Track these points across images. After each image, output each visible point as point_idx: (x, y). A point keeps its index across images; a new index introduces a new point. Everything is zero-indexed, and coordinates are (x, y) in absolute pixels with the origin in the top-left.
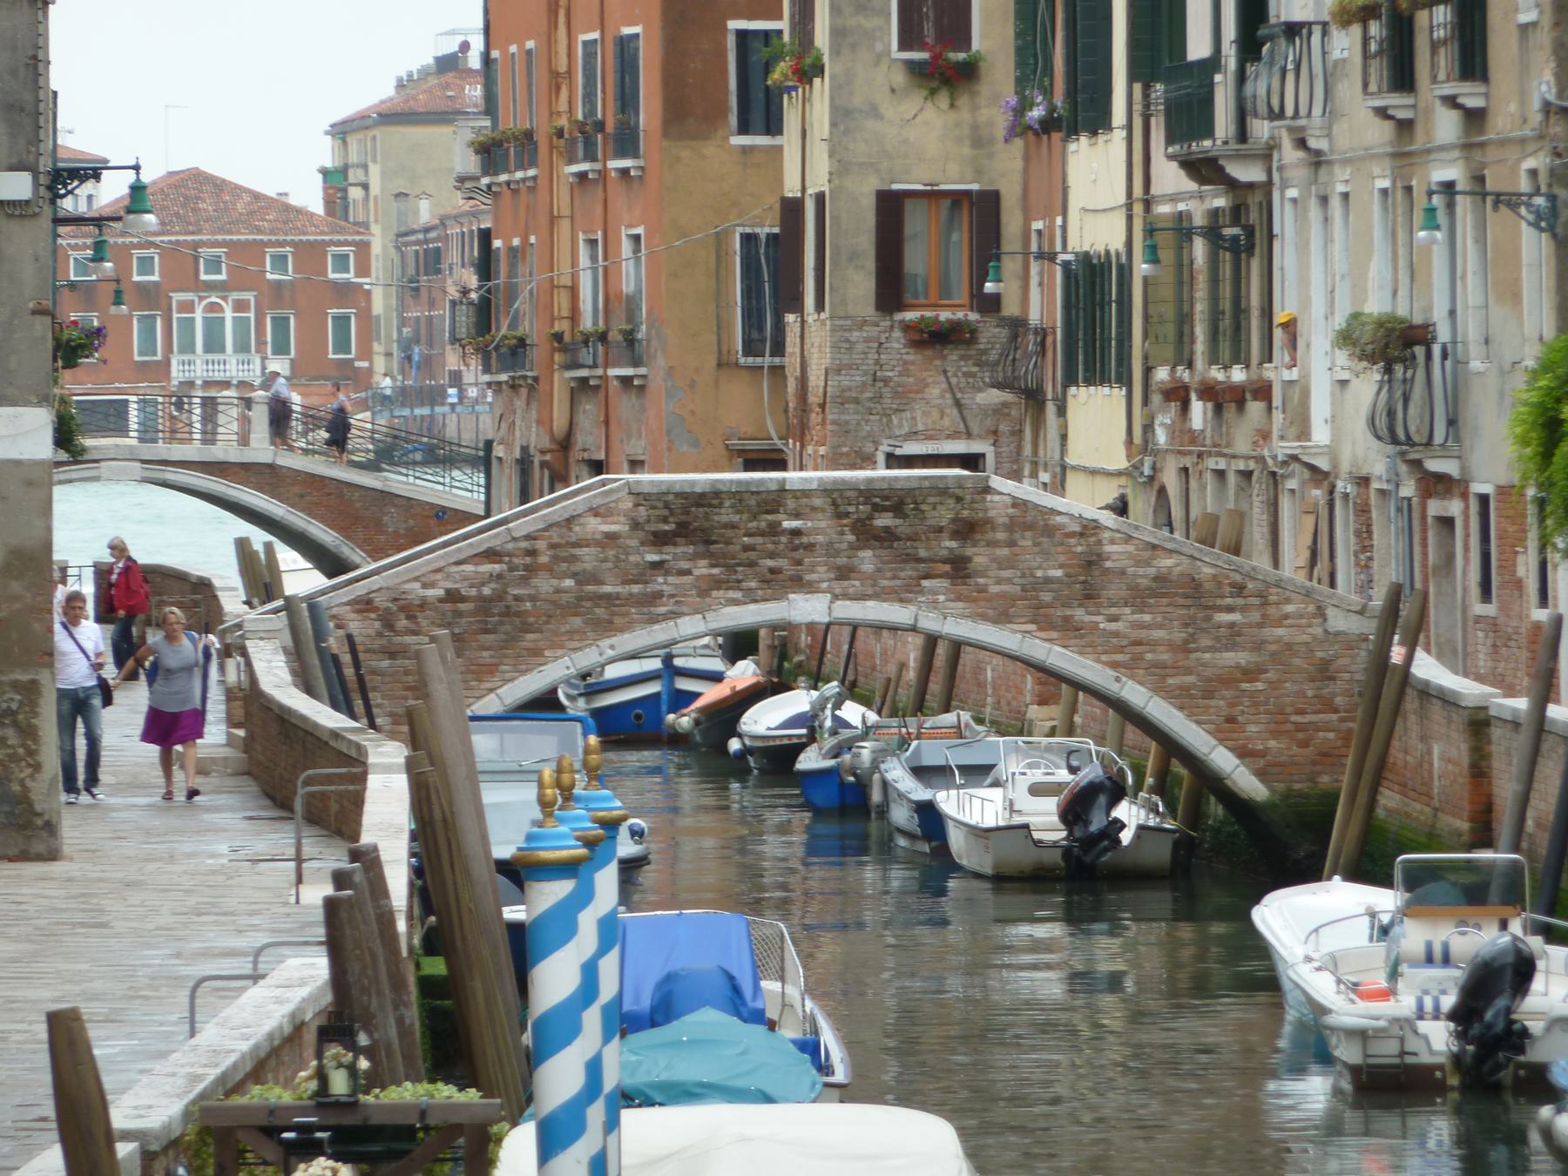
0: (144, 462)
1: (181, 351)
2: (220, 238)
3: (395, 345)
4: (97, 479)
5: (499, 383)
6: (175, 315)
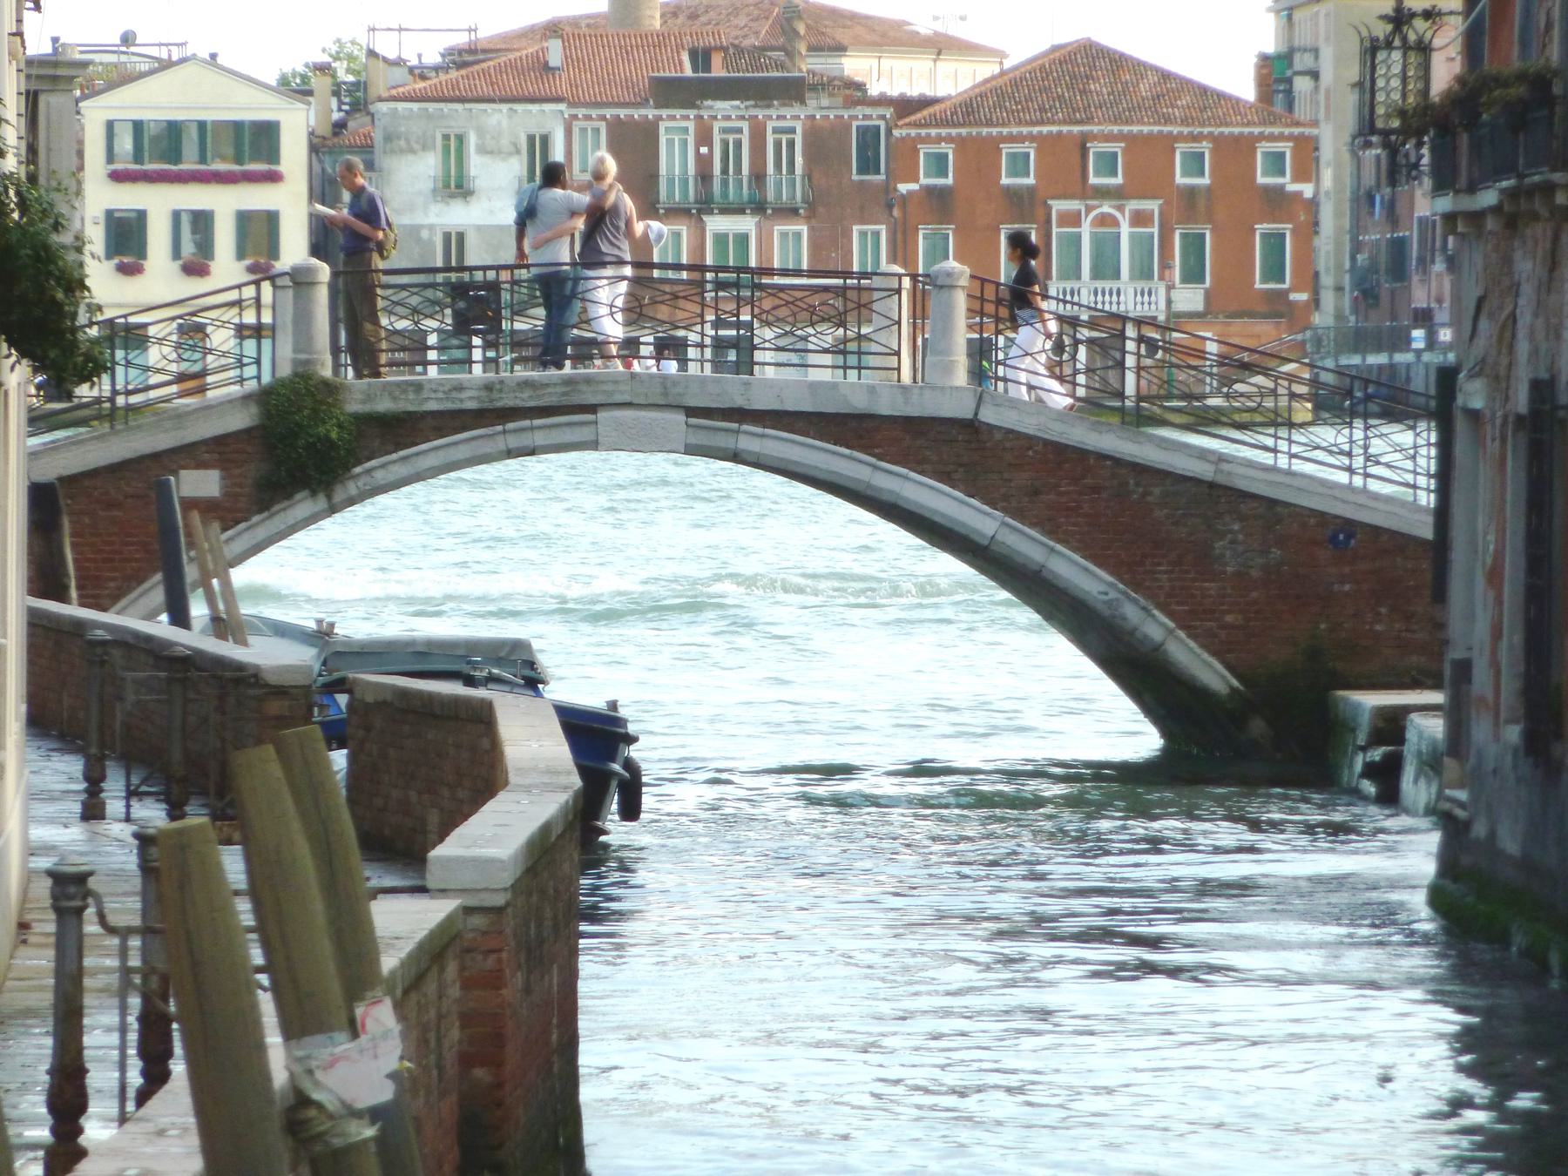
0: (691, 412)
1: (1062, 277)
2: (1116, 129)
3: (1347, 277)
4: (594, 445)
5: (1476, 217)
6: (1055, 230)
